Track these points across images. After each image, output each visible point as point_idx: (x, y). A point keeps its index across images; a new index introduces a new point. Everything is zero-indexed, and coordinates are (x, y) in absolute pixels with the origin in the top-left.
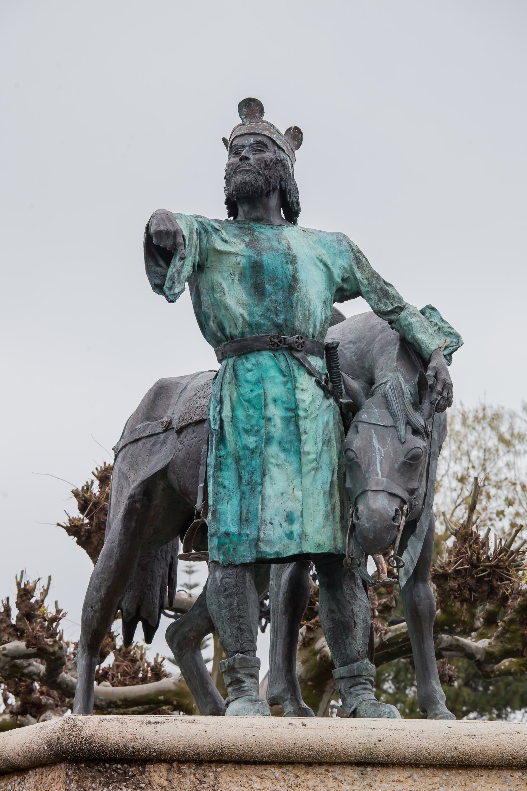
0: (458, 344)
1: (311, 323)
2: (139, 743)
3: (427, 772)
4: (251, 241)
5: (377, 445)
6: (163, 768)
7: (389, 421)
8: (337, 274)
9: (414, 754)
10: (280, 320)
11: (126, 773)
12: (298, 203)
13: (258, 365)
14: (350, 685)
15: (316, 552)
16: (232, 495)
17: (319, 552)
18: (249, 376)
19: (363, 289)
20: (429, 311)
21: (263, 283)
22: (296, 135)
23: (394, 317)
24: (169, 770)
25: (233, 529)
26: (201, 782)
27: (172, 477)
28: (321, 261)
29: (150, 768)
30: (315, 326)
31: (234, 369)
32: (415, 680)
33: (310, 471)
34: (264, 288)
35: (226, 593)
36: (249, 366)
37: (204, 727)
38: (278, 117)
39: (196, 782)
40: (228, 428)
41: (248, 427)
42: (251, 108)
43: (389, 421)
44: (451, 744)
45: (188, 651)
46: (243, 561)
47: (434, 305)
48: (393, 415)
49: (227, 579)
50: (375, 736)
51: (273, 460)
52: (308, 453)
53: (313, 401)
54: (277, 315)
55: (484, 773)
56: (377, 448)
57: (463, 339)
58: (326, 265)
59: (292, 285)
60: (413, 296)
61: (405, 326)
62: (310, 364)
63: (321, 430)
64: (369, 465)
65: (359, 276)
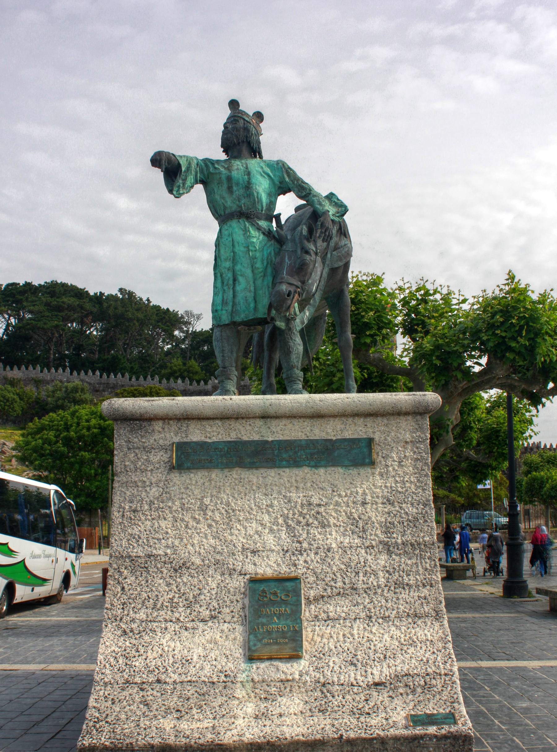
0: (346, 210)
2: (142, 411)
3: (300, 420)
5: (287, 260)
6: (160, 423)
8: (277, 180)
11: (141, 425)
19: (291, 186)
20: (331, 197)
22: (259, 116)
24: (163, 424)
26: (179, 429)
29: (154, 423)
38: (248, 107)
39: (177, 429)
42: (234, 104)
46: (224, 323)
47: (334, 192)
51: (239, 273)
52: (258, 268)
55: (332, 419)
57: (349, 207)
59: (248, 186)
60: (321, 188)
65: (287, 179)
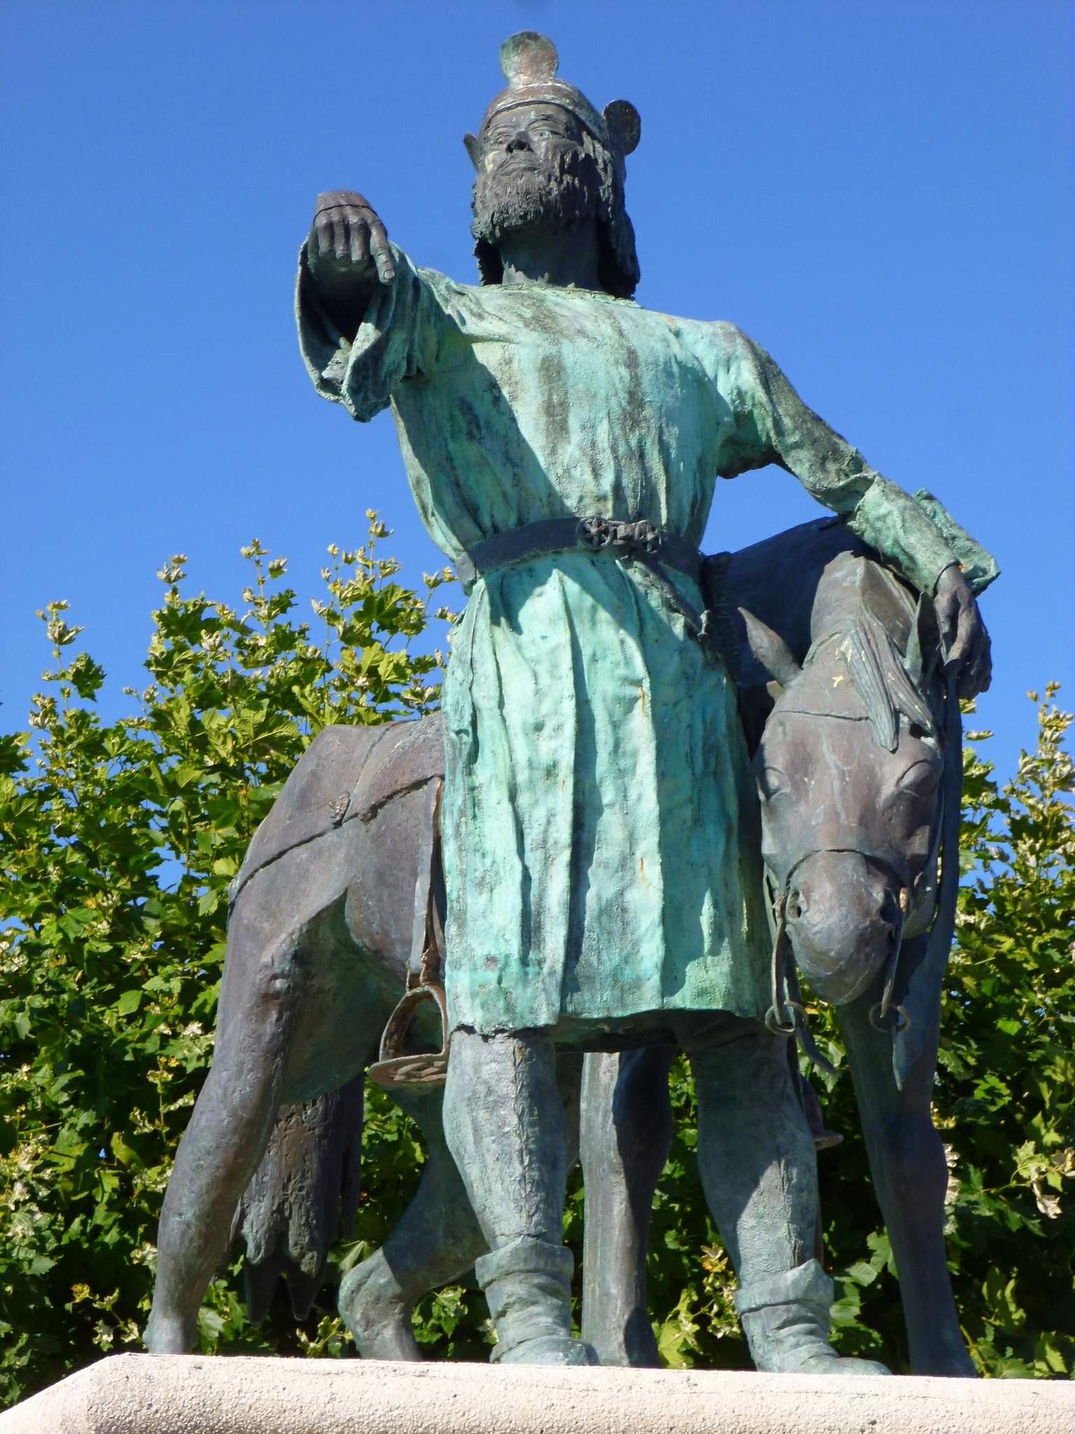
12: (634, 258)
14: (778, 1323)
15: (695, 1007)
16: (502, 873)
17: (704, 1007)
27: (351, 916)
31: (502, 594)
35: (490, 1099)
40: (489, 725)
45: (385, 1327)
49: (493, 1065)
56: (831, 764)
61: (878, 518)
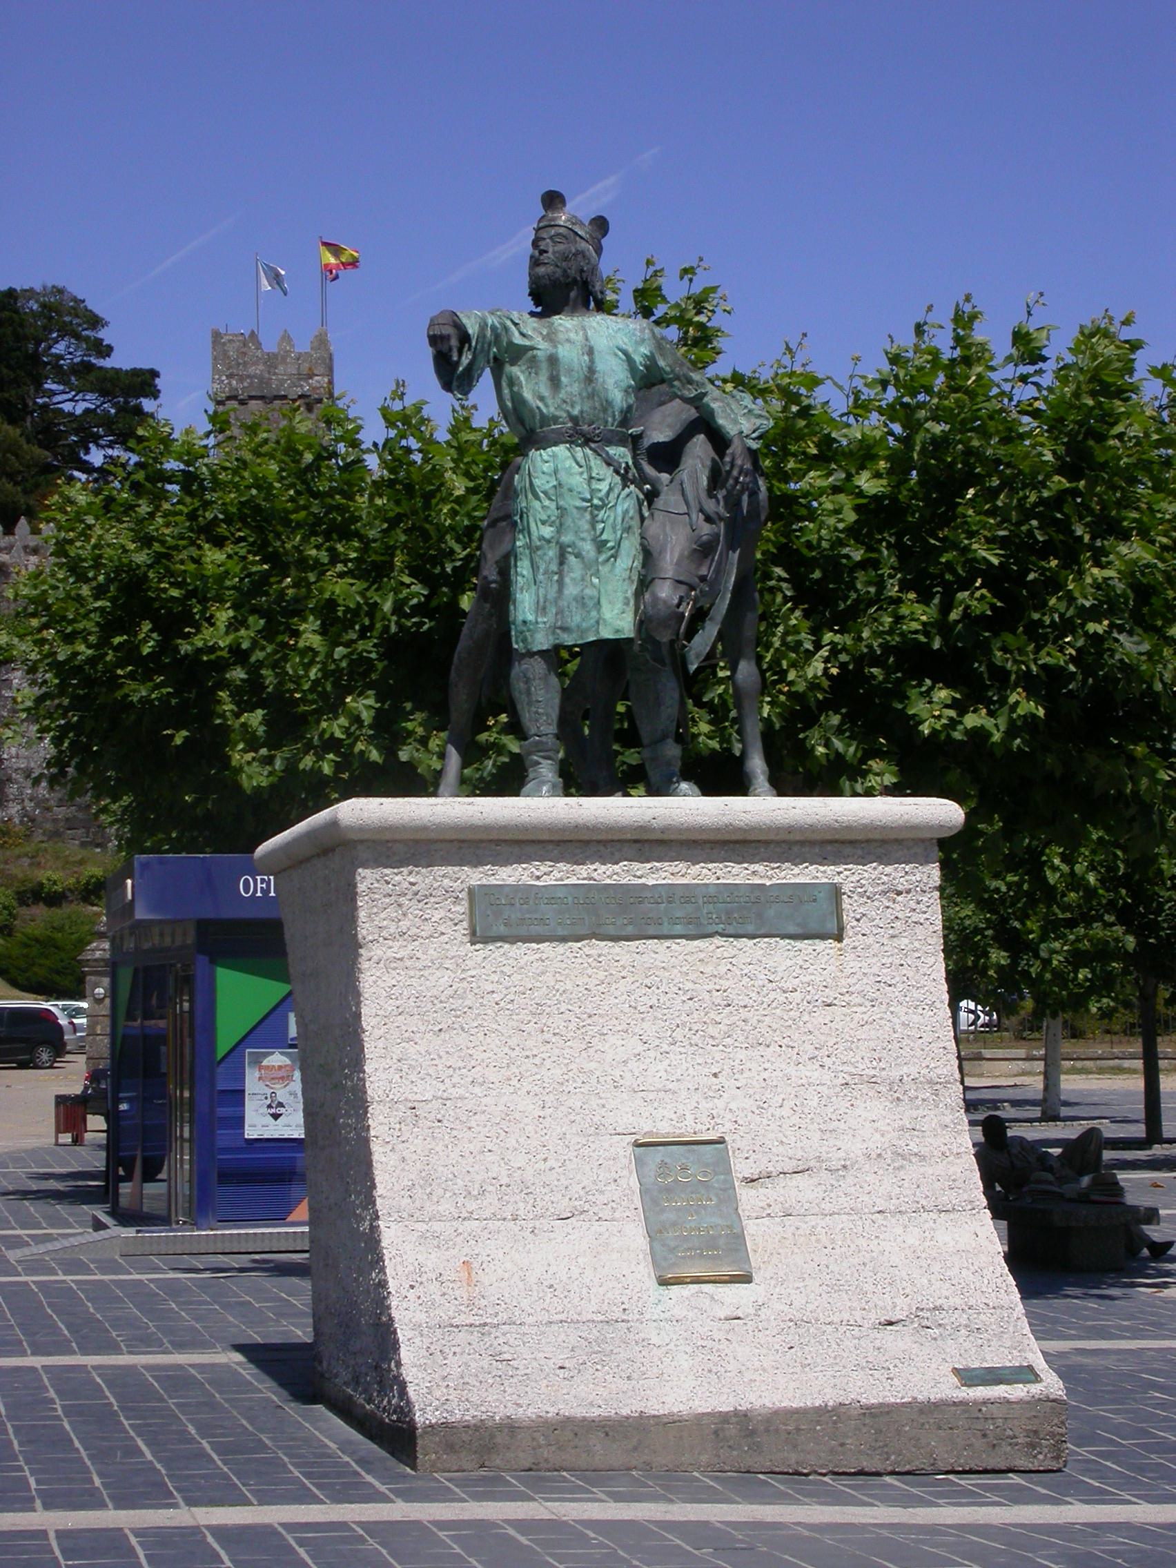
1: (610, 412)
4: (548, 334)
7: (684, 509)
9: (664, 830)
10: (576, 412)
13: (554, 456)
18: (546, 467)
21: (558, 375)
23: (698, 404)
25: (530, 617)
28: (621, 350)
30: (614, 416)
32: (269, 750)
33: (608, 560)
34: (559, 380)
36: (546, 457)
37: (480, 809)
41: (544, 517)
43: (684, 509)
44: (725, 820)
46: (540, 648)
48: (687, 503)
50: (648, 815)
53: (611, 489)
54: (572, 406)
58: (625, 353)
62: (607, 453)
63: (619, 519)
64: (660, 553)
